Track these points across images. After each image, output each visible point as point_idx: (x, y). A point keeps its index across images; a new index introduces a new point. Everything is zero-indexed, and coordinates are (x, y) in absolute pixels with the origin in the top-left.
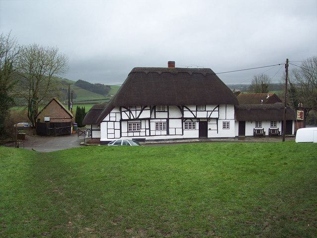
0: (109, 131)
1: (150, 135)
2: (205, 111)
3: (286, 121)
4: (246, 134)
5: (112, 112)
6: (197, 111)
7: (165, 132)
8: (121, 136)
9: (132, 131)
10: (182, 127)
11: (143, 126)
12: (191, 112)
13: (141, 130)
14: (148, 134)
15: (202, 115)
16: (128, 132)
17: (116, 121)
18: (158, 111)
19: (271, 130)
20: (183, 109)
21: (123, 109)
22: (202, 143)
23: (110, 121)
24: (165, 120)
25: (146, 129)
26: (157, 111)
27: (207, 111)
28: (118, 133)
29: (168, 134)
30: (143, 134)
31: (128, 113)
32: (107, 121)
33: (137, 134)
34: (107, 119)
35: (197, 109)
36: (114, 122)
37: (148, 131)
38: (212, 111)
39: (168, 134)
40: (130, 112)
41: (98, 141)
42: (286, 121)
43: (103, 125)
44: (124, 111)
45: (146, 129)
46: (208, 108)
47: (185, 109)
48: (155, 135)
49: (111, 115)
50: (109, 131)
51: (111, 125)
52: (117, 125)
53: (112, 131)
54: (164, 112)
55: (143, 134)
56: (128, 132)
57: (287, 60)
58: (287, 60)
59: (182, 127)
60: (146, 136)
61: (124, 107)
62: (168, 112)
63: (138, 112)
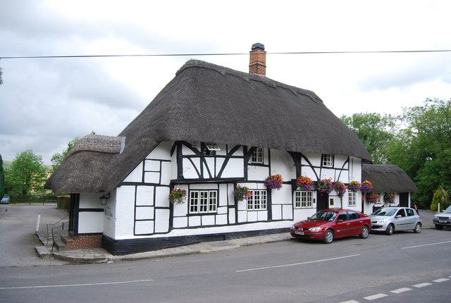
1: (237, 223)
2: (333, 168)
4: (80, 231)
5: (150, 156)
6: (321, 167)
7: (263, 215)
8: (171, 227)
9: (199, 211)
11: (223, 201)
12: (313, 167)
13: (220, 210)
14: (232, 220)
15: (328, 175)
16: (188, 215)
17: (159, 185)
18: (252, 164)
20: (300, 161)
21: (186, 151)
22: (10, 265)
23: (143, 183)
24: (261, 186)
25: (229, 207)
27: (336, 169)
28: (163, 216)
29: (270, 219)
30: (221, 220)
31: (197, 161)
32: (136, 184)
33: (208, 220)
34: (135, 176)
35: (321, 165)
36: (155, 185)
37: (232, 211)
39: (270, 219)
40: (203, 160)
41: (106, 243)
43: (124, 195)
44: (189, 157)
46: (338, 164)
47: (303, 162)
48: (282, 220)
49: (150, 165)
51: (145, 194)
52: (164, 193)
53: (148, 213)
54: (263, 165)
56: (188, 215)
57: (258, 49)
58: (258, 49)
59: (293, 204)
60: (228, 224)
61: (189, 146)
62: (269, 166)
63: (220, 161)
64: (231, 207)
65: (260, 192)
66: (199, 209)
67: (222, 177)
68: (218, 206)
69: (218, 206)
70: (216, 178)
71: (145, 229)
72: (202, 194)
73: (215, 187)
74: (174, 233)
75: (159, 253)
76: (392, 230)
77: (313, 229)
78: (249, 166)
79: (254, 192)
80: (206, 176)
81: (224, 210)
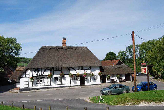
0: (25, 83)
1: (51, 85)
2: (83, 70)
3: (104, 71)
6: (78, 70)
10: (70, 80)
12: (75, 70)
13: (45, 82)
14: (49, 84)
18: (56, 71)
19: (112, 79)
23: (26, 77)
26: (55, 70)
29: (62, 84)
30: (46, 84)
32: (24, 77)
34: (24, 76)
37: (49, 82)
38: (87, 70)
39: (62, 84)
42: (104, 71)
44: (34, 71)
45: (48, 81)
49: (27, 73)
50: (25, 83)
51: (26, 79)
53: (27, 83)
54: (59, 71)
55: (45, 84)
59: (70, 80)
60: (48, 85)
62: (61, 71)
64: (49, 81)
65: (56, 78)
66: (40, 82)
67: (43, 75)
68: (45, 81)
69: (45, 81)
70: (41, 75)
71: (26, 86)
72: (40, 79)
73: (44, 77)
74: (33, 87)
75: (28, 91)
76: (45, 70)
77: (104, 91)
78: (54, 71)
79: (56, 78)
80: (39, 75)
81: (47, 82)
